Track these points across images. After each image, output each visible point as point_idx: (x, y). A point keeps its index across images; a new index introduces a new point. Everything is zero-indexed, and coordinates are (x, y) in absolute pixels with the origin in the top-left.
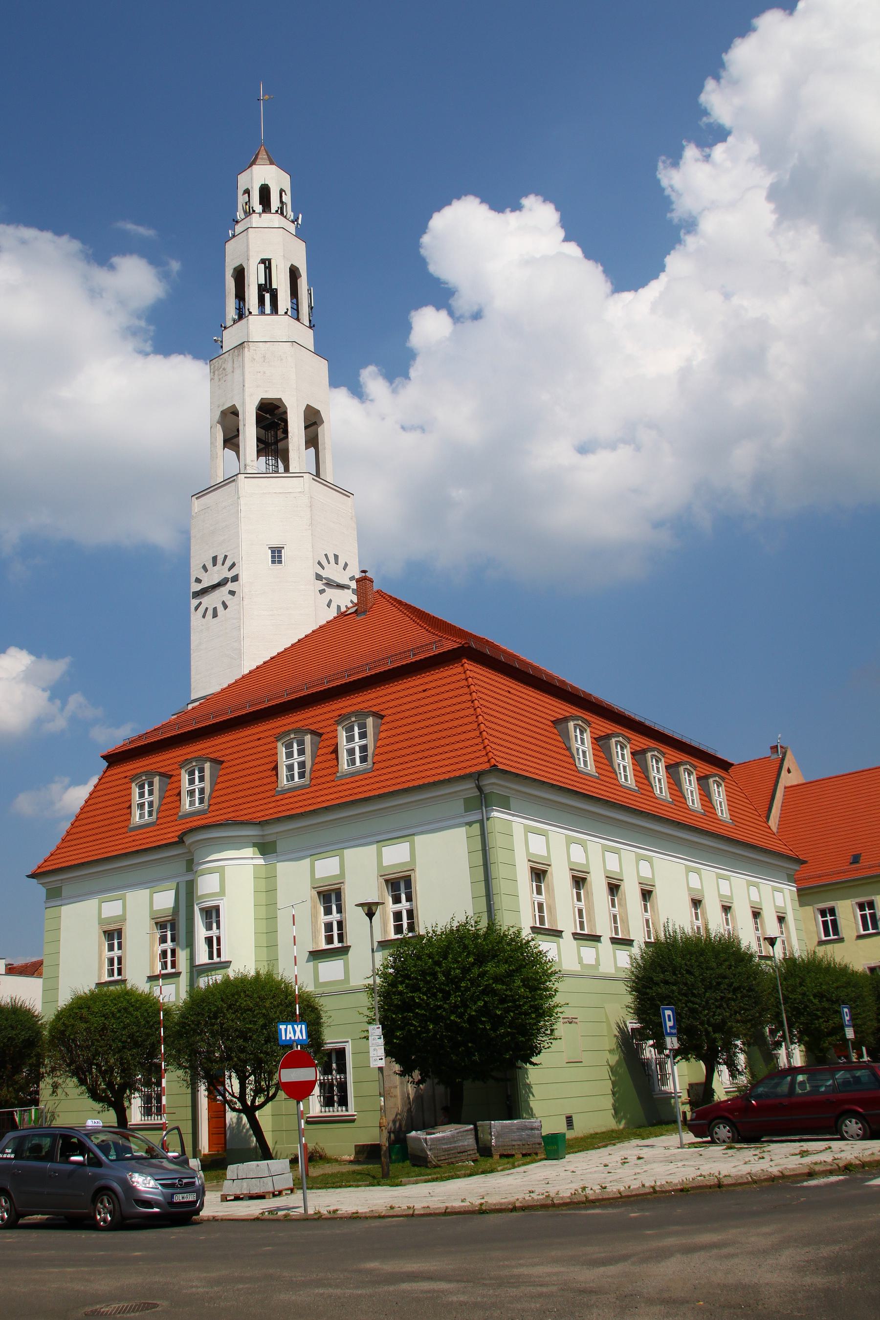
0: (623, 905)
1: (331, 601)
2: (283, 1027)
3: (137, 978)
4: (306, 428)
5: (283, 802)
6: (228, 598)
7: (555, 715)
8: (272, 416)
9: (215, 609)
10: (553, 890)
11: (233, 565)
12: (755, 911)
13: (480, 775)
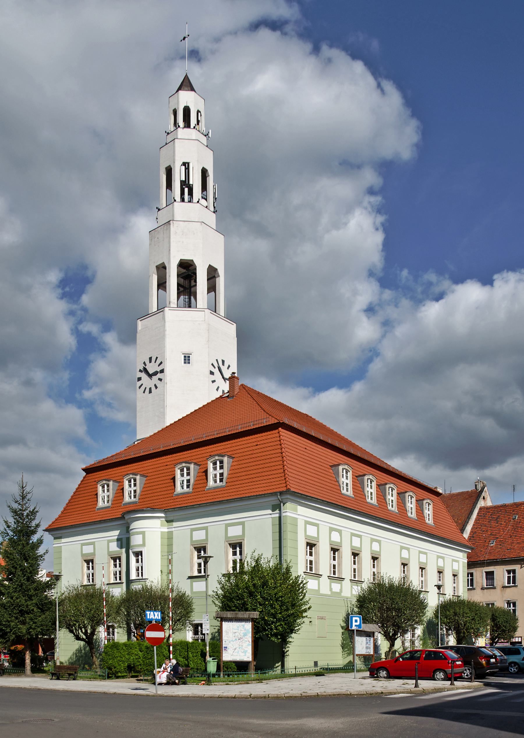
0: (360, 563)
1: (218, 387)
2: (148, 613)
3: (100, 582)
4: (208, 280)
5: (177, 500)
6: (158, 383)
7: (333, 462)
8: (187, 269)
9: (150, 389)
10: (319, 554)
11: (161, 363)
12: (437, 571)
13: (281, 493)
